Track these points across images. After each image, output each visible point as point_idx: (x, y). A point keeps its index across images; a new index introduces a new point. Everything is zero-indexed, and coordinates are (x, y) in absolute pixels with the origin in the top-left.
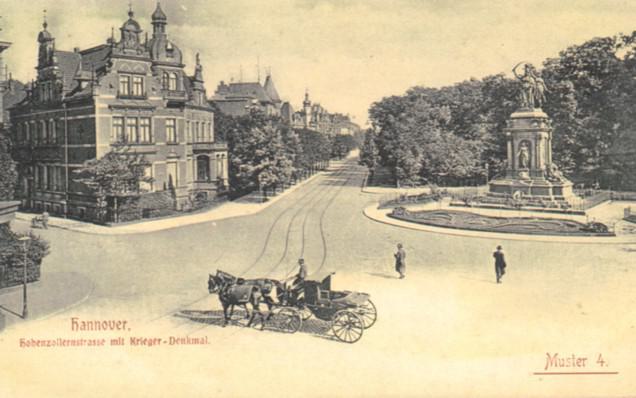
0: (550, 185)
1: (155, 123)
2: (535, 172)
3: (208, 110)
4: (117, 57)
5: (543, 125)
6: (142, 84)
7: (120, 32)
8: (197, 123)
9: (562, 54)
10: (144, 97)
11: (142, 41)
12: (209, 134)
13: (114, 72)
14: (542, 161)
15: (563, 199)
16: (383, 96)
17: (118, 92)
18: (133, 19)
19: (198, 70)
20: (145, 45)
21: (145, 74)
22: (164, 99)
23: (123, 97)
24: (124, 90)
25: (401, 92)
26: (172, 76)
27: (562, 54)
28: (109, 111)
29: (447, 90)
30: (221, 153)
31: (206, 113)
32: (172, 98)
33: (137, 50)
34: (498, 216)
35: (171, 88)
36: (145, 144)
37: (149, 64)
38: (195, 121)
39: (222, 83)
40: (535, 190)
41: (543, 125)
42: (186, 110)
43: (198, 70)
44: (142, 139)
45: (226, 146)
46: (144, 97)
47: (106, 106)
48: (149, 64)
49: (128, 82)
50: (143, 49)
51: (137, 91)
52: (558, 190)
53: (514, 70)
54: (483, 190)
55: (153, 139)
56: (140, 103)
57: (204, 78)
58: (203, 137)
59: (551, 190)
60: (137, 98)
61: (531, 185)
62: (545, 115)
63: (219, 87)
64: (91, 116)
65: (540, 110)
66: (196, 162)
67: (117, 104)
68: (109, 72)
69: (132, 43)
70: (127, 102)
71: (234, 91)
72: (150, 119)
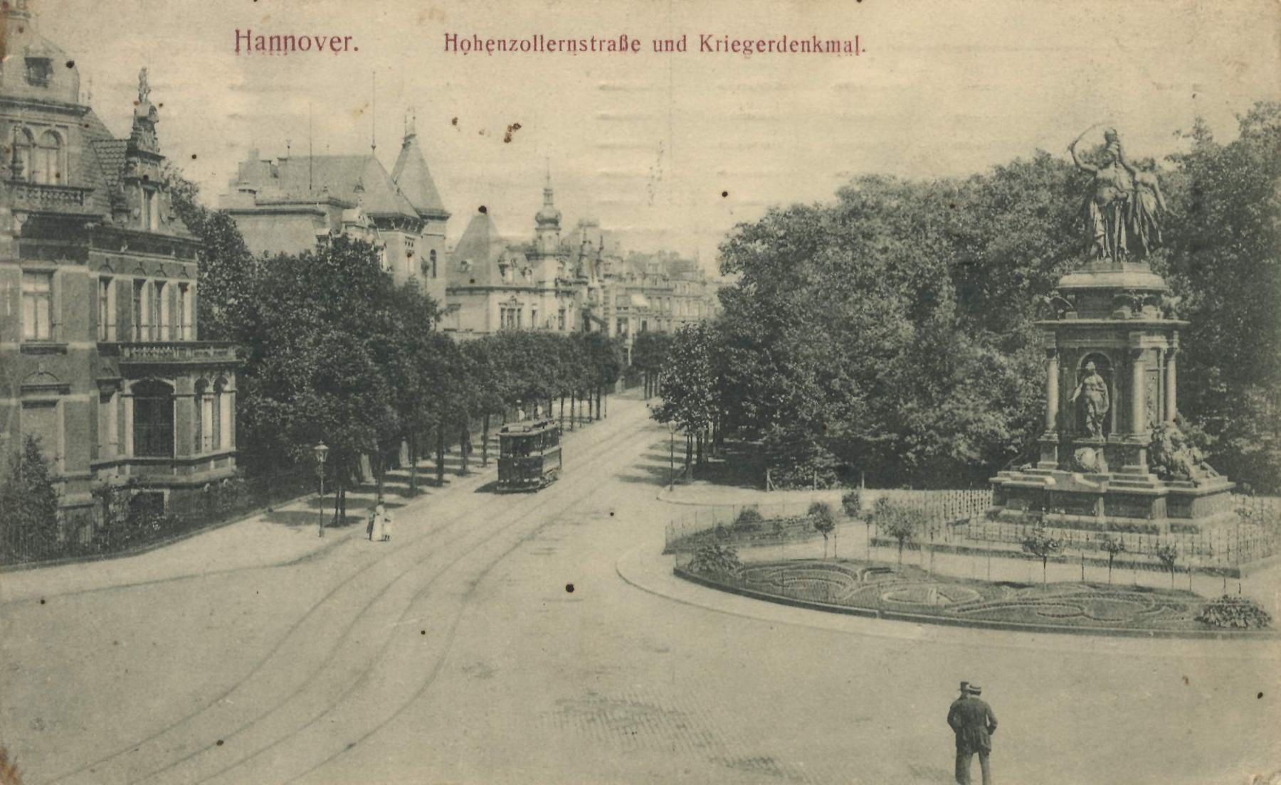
0: (1162, 490)
19: (145, 122)
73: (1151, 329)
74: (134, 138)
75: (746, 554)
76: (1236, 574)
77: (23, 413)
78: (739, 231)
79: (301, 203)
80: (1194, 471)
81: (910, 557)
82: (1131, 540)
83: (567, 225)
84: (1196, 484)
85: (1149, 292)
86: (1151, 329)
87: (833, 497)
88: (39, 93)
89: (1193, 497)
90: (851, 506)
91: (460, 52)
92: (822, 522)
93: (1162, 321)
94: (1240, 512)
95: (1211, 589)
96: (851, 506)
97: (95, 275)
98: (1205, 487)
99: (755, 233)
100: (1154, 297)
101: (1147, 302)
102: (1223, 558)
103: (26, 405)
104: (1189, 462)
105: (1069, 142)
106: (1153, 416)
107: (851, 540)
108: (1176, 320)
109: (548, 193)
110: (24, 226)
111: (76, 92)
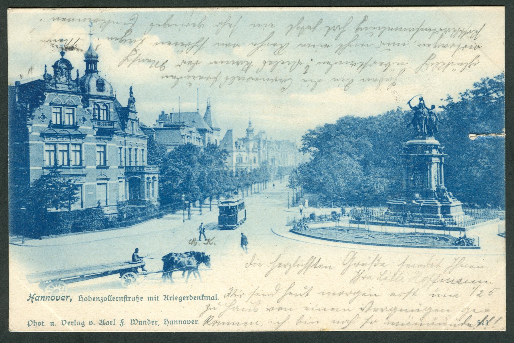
0: (439, 205)
1: (85, 148)
2: (427, 194)
3: (142, 138)
4: (50, 91)
5: (435, 152)
6: (73, 114)
7: (52, 69)
8: (130, 149)
9: (475, 85)
10: (75, 127)
11: (74, 77)
12: (141, 158)
13: (47, 104)
14: (434, 183)
15: (451, 217)
16: (309, 128)
17: (51, 121)
18: (65, 57)
19: (132, 101)
20: (77, 81)
21: (76, 106)
22: (94, 128)
23: (56, 126)
24: (55, 120)
25: (333, 121)
26: (101, 106)
27: (475, 85)
28: (41, 138)
29: (370, 120)
30: (151, 176)
31: (140, 141)
32: (101, 126)
33: (68, 85)
34: (134, 157)
35: (102, 118)
36: (75, 167)
37: (80, 97)
38: (127, 147)
39: (163, 112)
40: (424, 209)
41: (435, 152)
42: (115, 137)
43: (132, 101)
44: (72, 163)
45: (158, 169)
46: (75, 127)
47: (39, 134)
48: (80, 97)
49: (61, 113)
50: (74, 84)
51: (68, 120)
52: (446, 210)
53: (409, 103)
54: (379, 211)
55: (84, 162)
56: (72, 131)
57: (137, 109)
58: (136, 162)
59: (439, 209)
60: (69, 127)
61: (422, 204)
62: (437, 142)
63: (160, 116)
64: (27, 142)
65: (433, 138)
66: (128, 183)
67: (50, 132)
68: (42, 104)
69: (63, 79)
70: (58, 131)
71: (170, 124)
72: (80, 145)
73: (435, 156)
74: (129, 107)
75: (311, 225)
76: (464, 230)
77: (97, 186)
78: (309, 132)
79: (52, 298)
80: (450, 199)
81: (361, 226)
82: (430, 220)
83: (256, 133)
84: (451, 203)
85: (435, 145)
86: (435, 156)
87: (338, 210)
88: (100, 94)
89: (450, 206)
90: (343, 212)
91: (175, 296)
92: (335, 217)
93: (439, 154)
94: (204, 38)
95: (456, 234)
96: (343, 212)
97: (118, 147)
98: (454, 204)
99: (313, 133)
100: (436, 147)
101: (434, 148)
102: (460, 225)
103: (98, 184)
104: (448, 196)
105: (408, 101)
106: (437, 183)
107: (344, 222)
108: (443, 154)
109: (250, 123)
110: (97, 132)
111: (111, 93)
